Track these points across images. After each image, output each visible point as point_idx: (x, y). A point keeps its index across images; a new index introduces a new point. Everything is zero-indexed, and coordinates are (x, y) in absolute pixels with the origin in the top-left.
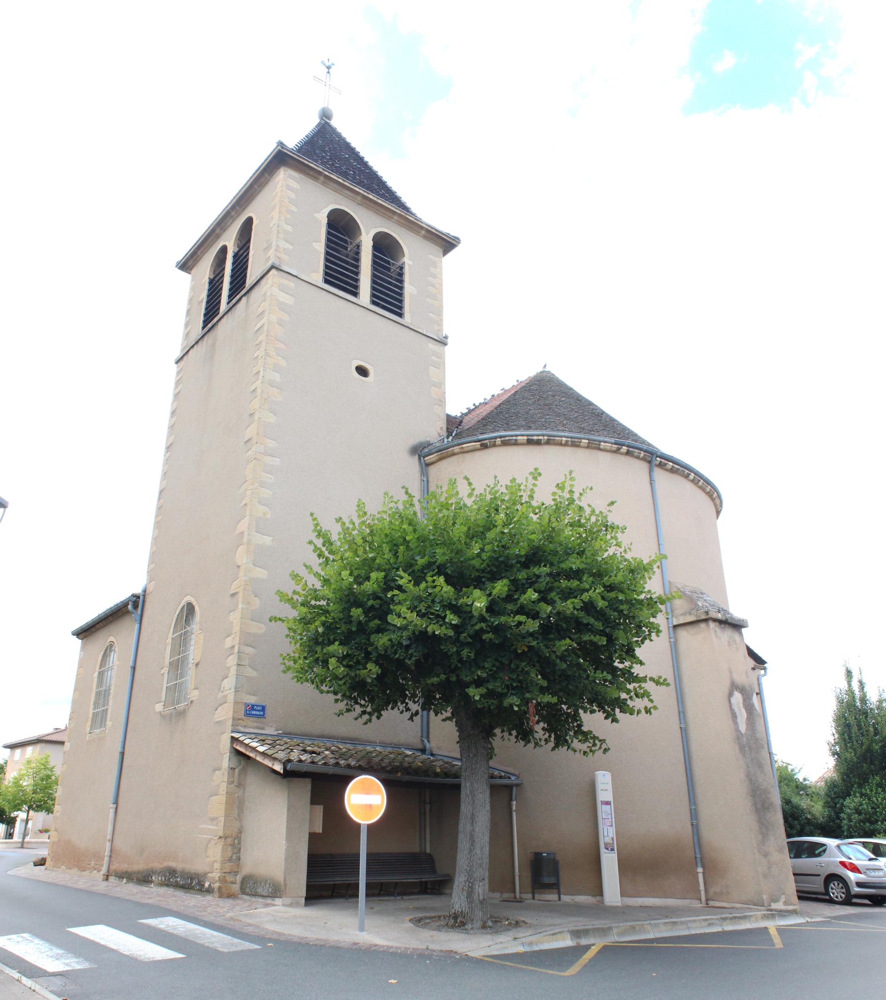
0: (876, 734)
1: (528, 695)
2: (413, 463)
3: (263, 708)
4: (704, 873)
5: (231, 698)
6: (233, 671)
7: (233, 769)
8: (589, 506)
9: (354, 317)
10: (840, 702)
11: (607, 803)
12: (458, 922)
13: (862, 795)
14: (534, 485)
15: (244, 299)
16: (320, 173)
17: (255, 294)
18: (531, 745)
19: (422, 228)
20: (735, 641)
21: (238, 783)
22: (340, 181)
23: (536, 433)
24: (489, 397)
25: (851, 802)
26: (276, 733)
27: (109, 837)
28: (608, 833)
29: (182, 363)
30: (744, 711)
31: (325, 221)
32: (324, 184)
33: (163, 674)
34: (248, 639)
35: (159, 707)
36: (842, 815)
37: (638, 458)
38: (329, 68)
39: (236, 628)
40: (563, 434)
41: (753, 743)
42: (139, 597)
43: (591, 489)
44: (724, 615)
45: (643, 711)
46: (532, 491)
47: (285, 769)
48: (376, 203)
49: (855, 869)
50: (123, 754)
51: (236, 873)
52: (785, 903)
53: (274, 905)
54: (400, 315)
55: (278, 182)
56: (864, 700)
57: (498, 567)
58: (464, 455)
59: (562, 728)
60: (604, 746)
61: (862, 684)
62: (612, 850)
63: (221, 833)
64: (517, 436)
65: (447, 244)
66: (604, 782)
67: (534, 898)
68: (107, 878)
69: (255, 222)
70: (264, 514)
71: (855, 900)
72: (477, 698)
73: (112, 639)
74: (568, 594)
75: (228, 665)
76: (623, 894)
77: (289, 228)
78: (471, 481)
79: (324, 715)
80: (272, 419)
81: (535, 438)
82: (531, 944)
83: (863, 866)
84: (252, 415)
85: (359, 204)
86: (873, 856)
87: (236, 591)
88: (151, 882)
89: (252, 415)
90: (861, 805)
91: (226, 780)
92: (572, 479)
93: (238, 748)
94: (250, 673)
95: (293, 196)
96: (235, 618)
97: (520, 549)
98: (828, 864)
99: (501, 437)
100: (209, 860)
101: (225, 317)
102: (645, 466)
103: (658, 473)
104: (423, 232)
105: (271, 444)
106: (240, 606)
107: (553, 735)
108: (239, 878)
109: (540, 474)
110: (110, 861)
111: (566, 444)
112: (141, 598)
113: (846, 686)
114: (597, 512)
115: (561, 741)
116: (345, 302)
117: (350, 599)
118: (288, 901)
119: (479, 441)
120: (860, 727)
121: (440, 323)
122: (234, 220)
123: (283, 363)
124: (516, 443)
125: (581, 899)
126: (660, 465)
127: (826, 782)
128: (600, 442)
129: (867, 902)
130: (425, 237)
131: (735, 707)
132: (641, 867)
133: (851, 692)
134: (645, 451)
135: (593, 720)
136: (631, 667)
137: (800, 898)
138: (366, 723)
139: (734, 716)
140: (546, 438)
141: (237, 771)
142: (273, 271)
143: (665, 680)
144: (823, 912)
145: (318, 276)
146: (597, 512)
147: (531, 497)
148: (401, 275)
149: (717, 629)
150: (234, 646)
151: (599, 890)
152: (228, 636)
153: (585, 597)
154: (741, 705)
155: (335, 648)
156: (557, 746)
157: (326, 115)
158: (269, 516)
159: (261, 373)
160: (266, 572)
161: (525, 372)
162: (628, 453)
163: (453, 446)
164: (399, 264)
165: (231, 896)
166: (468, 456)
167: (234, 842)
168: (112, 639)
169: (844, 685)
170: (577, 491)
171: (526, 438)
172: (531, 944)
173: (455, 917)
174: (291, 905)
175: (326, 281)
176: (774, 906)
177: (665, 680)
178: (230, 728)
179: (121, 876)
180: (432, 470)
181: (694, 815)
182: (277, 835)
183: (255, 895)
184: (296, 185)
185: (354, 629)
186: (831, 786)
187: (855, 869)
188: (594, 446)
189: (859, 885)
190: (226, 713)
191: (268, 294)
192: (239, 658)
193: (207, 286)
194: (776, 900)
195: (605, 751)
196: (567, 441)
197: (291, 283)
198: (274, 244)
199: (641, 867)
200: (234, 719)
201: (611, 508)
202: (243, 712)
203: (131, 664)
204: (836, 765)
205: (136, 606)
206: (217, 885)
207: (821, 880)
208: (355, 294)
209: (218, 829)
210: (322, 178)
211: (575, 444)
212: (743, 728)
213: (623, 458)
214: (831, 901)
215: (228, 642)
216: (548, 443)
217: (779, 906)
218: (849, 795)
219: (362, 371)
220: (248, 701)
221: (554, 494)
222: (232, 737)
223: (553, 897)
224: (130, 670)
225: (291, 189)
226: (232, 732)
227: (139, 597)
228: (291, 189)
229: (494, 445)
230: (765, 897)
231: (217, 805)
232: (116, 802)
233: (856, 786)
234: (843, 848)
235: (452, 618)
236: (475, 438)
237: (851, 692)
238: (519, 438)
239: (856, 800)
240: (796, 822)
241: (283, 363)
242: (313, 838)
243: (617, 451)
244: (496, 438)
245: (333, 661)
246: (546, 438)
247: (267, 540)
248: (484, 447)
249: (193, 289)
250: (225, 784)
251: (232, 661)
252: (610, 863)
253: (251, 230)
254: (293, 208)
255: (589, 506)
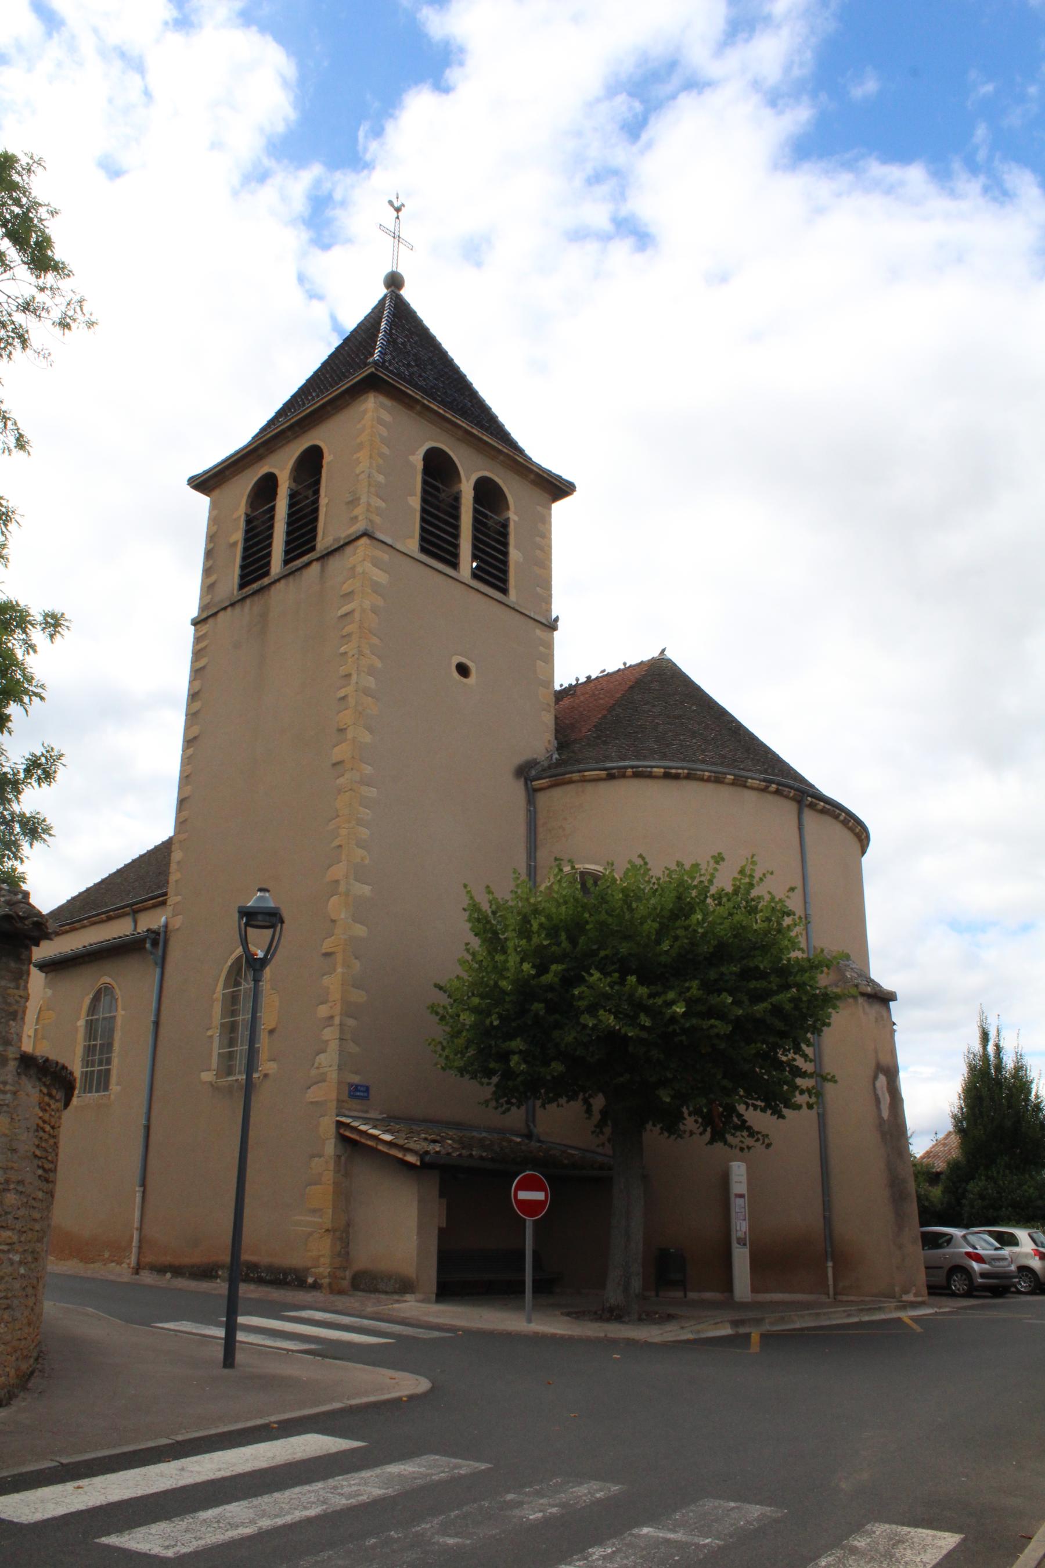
0: (1009, 1108)
1: (712, 1096)
2: (518, 790)
3: (367, 1089)
4: (834, 1268)
5: (333, 1075)
6: (334, 1046)
7: (339, 1157)
8: (769, 893)
9: (452, 592)
10: (972, 1068)
11: (742, 1196)
12: (614, 1314)
13: (988, 1178)
14: (716, 869)
15: (316, 567)
16: (417, 401)
17: (334, 564)
18: (673, 1137)
19: (531, 471)
20: (882, 1017)
21: (344, 1169)
22: (441, 411)
23: (677, 766)
24: (582, 680)
25: (974, 1187)
26: (380, 1117)
27: (136, 1224)
28: (740, 1226)
29: (205, 628)
30: (887, 1096)
31: (420, 465)
32: (420, 414)
33: (211, 1037)
34: (350, 1010)
35: (207, 1076)
36: (964, 1201)
37: (787, 797)
38: (398, 210)
39: (336, 995)
40: (704, 767)
41: (893, 1128)
42: (158, 934)
43: (772, 873)
44: (874, 988)
45: (805, 1106)
46: (713, 876)
47: (422, 1161)
48: (480, 440)
49: (979, 1259)
50: (148, 1128)
51: (345, 1269)
52: (916, 1295)
53: (406, 1301)
54: (504, 591)
55: (365, 412)
56: (999, 1067)
57: (686, 964)
58: (585, 784)
59: (722, 1126)
60: (767, 1141)
61: (998, 1049)
62: (745, 1245)
63: (329, 1226)
64: (652, 767)
65: (558, 488)
66: (739, 1171)
67: (657, 1296)
68: (137, 1271)
69: (328, 458)
70: (362, 859)
71: (976, 1293)
72: (668, 1100)
73: (107, 979)
74: (757, 997)
75: (325, 1038)
76: (754, 1290)
77: (381, 478)
78: (647, 860)
79: (470, 1099)
80: (367, 738)
81: (673, 771)
82: (698, 1332)
83: (987, 1255)
84: (342, 731)
85: (458, 439)
86: (998, 1245)
87: (329, 950)
88: (217, 1277)
89: (342, 731)
90: (986, 1189)
91: (332, 1168)
92: (754, 863)
93: (348, 1134)
94: (354, 1049)
95: (384, 432)
96: (333, 983)
97: (705, 949)
98: (953, 1255)
99: (632, 767)
100: (317, 1255)
101: (283, 582)
102: (793, 806)
103: (809, 816)
104: (532, 476)
105: (368, 770)
106: (339, 970)
107: (709, 1129)
108: (348, 1274)
109: (723, 859)
110: (139, 1253)
111: (708, 780)
112: (162, 935)
113: (981, 1050)
114: (777, 900)
115: (718, 1136)
116: (444, 577)
117: (526, 991)
118: (420, 1296)
119: (605, 769)
120: (992, 1099)
121: (547, 599)
122: (289, 442)
123: (379, 664)
124: (650, 776)
125: (708, 1295)
126: (812, 806)
127: (949, 1164)
128: (747, 778)
129: (989, 1294)
130: (533, 483)
131: (879, 1093)
132: (776, 1262)
133: (985, 1056)
134: (796, 790)
135: (757, 1118)
136: (794, 1060)
137: (930, 1294)
138: (504, 1113)
139: (878, 1101)
140: (686, 771)
141: (343, 1158)
142: (364, 540)
143: (833, 1077)
144: (947, 1306)
145: (413, 545)
146: (777, 900)
147: (711, 881)
148: (505, 535)
149: (866, 1006)
150: (332, 1017)
151: (727, 1284)
152: (322, 1003)
153: (775, 999)
154: (885, 1089)
155: (517, 1044)
156: (711, 1142)
157: (394, 282)
158: (367, 862)
159: (354, 677)
160: (364, 928)
161: (638, 652)
162: (777, 792)
163: (572, 773)
164: (501, 519)
165: (341, 1292)
166: (589, 787)
167: (344, 1235)
168: (107, 979)
169: (977, 1047)
170: (758, 875)
171: (662, 770)
172: (698, 1332)
173: (611, 1310)
174: (422, 1301)
175: (423, 550)
176: (905, 1298)
177: (833, 1077)
178: (334, 1112)
179: (161, 1270)
180: (542, 798)
181: (827, 1205)
182: (400, 1227)
183: (376, 1291)
184: (386, 416)
185: (529, 1022)
186: (954, 1167)
187: (979, 1259)
188: (740, 783)
189: (983, 1275)
190: (327, 1092)
191: (359, 569)
192: (342, 1031)
193: (242, 524)
194: (907, 1292)
195: (768, 1146)
196: (710, 777)
197: (385, 556)
198: (364, 500)
199: (770, 1263)
200: (338, 1101)
201: (791, 894)
202: (347, 1093)
203: (153, 1018)
204: (962, 1143)
205: (155, 943)
206: (325, 1281)
207: (943, 1273)
208: (455, 566)
209: (327, 1220)
210: (418, 408)
211: (718, 780)
212: (885, 1114)
213: (770, 797)
214: (954, 1295)
215: (323, 1011)
216: (688, 777)
217: (910, 1297)
218: (973, 1178)
219: (463, 670)
220: (352, 1081)
221: (735, 879)
222: (338, 1121)
223: (679, 1294)
224: (151, 1026)
225: (380, 421)
226: (337, 1116)
227: (158, 934)
228: (380, 421)
229: (624, 776)
230: (897, 1289)
231: (322, 1194)
232: (143, 1184)
233: (982, 1168)
234: (970, 1238)
235: (645, 1020)
236: (601, 765)
237: (985, 1056)
238: (655, 770)
239: (980, 1184)
240: (929, 1215)
241: (379, 664)
242: (442, 1232)
243: (765, 790)
244: (626, 768)
245: (515, 1059)
246: (686, 771)
247: (366, 890)
248: (611, 777)
249: (215, 521)
250: (331, 1174)
251: (330, 1034)
252: (741, 1259)
253: (321, 466)
254: (385, 450)
255: (769, 893)
